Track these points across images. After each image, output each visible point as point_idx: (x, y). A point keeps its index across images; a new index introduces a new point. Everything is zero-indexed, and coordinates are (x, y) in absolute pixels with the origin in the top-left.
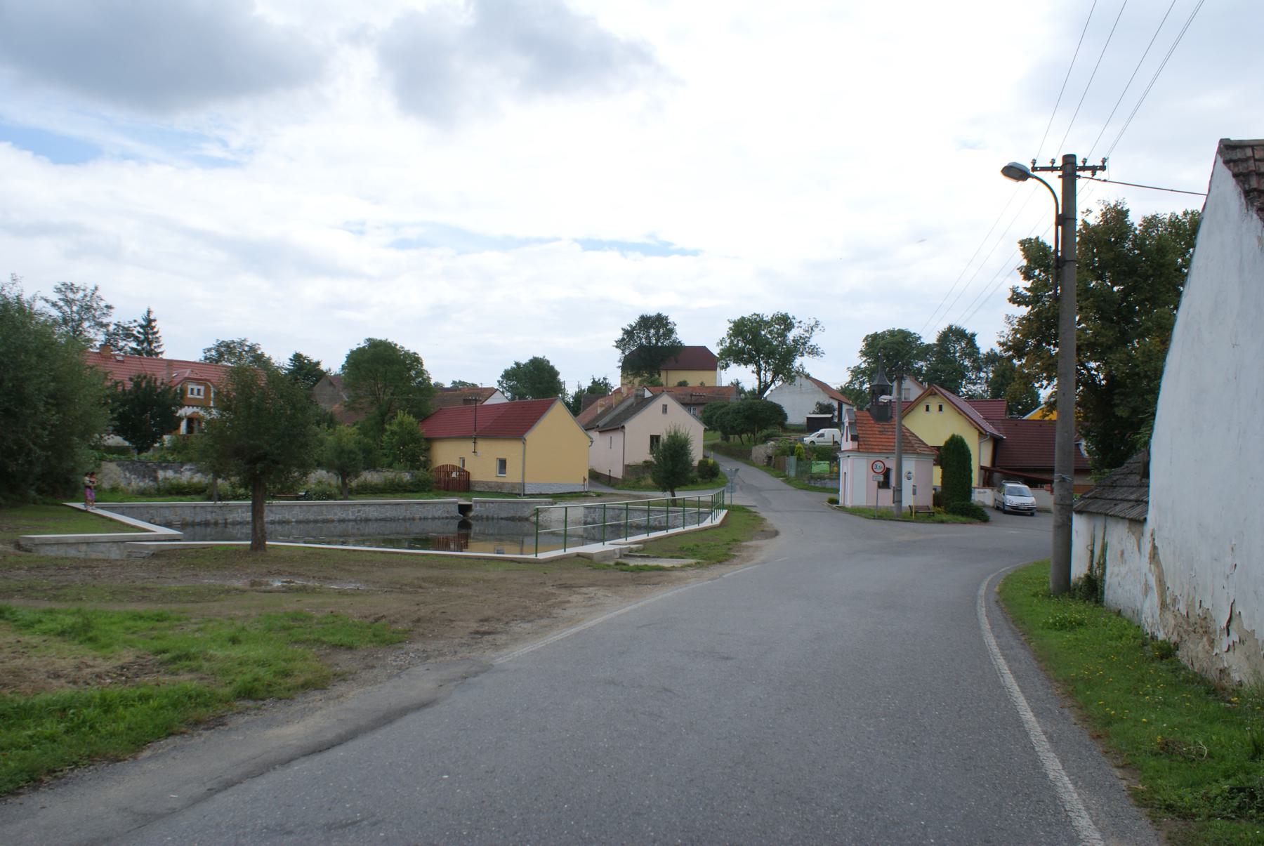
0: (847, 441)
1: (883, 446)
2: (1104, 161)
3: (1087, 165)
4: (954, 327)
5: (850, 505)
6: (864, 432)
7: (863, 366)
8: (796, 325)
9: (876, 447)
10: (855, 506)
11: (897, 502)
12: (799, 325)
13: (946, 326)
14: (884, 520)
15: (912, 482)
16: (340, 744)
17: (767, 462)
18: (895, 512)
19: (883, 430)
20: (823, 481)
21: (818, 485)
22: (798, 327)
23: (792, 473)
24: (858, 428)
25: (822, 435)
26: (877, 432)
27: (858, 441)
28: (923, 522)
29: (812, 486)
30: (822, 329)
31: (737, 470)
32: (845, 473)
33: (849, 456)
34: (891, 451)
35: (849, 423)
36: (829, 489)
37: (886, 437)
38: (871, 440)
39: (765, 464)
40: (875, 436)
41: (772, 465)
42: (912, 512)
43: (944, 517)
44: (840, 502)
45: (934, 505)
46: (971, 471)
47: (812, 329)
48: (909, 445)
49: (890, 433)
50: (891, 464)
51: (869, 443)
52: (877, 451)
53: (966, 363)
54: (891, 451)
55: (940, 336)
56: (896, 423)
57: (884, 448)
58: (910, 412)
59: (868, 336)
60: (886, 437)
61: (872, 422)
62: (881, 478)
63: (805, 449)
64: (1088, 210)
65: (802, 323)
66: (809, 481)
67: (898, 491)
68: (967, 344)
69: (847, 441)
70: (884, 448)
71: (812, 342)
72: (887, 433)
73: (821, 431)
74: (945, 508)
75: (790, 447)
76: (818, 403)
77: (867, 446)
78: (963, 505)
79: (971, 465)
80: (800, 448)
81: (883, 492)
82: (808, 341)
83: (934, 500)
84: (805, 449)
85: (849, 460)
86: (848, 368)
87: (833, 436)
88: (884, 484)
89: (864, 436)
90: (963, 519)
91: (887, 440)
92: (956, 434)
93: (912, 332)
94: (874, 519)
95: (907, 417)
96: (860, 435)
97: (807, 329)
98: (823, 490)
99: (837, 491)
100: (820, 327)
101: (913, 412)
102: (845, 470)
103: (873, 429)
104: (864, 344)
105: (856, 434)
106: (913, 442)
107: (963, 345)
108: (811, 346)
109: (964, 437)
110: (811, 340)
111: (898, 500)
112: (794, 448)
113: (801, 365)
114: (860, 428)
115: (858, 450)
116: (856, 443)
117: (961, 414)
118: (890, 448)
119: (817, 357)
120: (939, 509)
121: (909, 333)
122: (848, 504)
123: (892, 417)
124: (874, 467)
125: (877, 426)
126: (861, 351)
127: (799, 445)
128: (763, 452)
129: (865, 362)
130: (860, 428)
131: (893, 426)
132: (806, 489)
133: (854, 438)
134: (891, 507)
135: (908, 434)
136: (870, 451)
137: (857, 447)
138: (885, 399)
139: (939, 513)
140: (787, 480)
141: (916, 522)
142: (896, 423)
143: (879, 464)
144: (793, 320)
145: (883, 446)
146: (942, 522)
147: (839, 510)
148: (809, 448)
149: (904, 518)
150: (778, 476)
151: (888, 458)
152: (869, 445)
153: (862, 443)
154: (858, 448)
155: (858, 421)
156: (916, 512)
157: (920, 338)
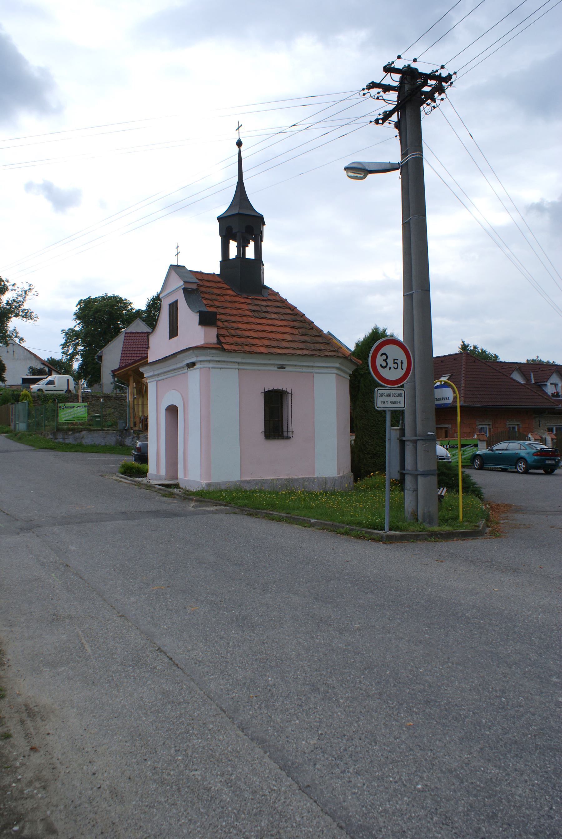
5: (204, 482)
8: (10, 288)
10: (215, 484)
12: (13, 288)
20: (77, 435)
21: (70, 440)
22: (12, 290)
23: (22, 426)
25: (51, 383)
27: (219, 328)
29: (59, 443)
30: (36, 293)
33: (193, 364)
38: (240, 326)
47: (26, 293)
51: (240, 333)
59: (81, 300)
63: (34, 397)
65: (16, 286)
71: (26, 306)
76: (31, 368)
77: (235, 339)
82: (22, 305)
84: (34, 397)
85: (194, 375)
86: (62, 331)
97: (20, 293)
100: (33, 291)
104: (77, 308)
108: (25, 310)
110: (25, 304)
113: (14, 330)
116: (213, 332)
119: (30, 321)
121: (121, 299)
126: (75, 314)
132: (52, 448)
136: (247, 348)
137: (215, 340)
144: (6, 283)
145: (269, 339)
148: (39, 396)
151: (282, 367)
152: (241, 337)
154: (219, 342)
157: (131, 303)
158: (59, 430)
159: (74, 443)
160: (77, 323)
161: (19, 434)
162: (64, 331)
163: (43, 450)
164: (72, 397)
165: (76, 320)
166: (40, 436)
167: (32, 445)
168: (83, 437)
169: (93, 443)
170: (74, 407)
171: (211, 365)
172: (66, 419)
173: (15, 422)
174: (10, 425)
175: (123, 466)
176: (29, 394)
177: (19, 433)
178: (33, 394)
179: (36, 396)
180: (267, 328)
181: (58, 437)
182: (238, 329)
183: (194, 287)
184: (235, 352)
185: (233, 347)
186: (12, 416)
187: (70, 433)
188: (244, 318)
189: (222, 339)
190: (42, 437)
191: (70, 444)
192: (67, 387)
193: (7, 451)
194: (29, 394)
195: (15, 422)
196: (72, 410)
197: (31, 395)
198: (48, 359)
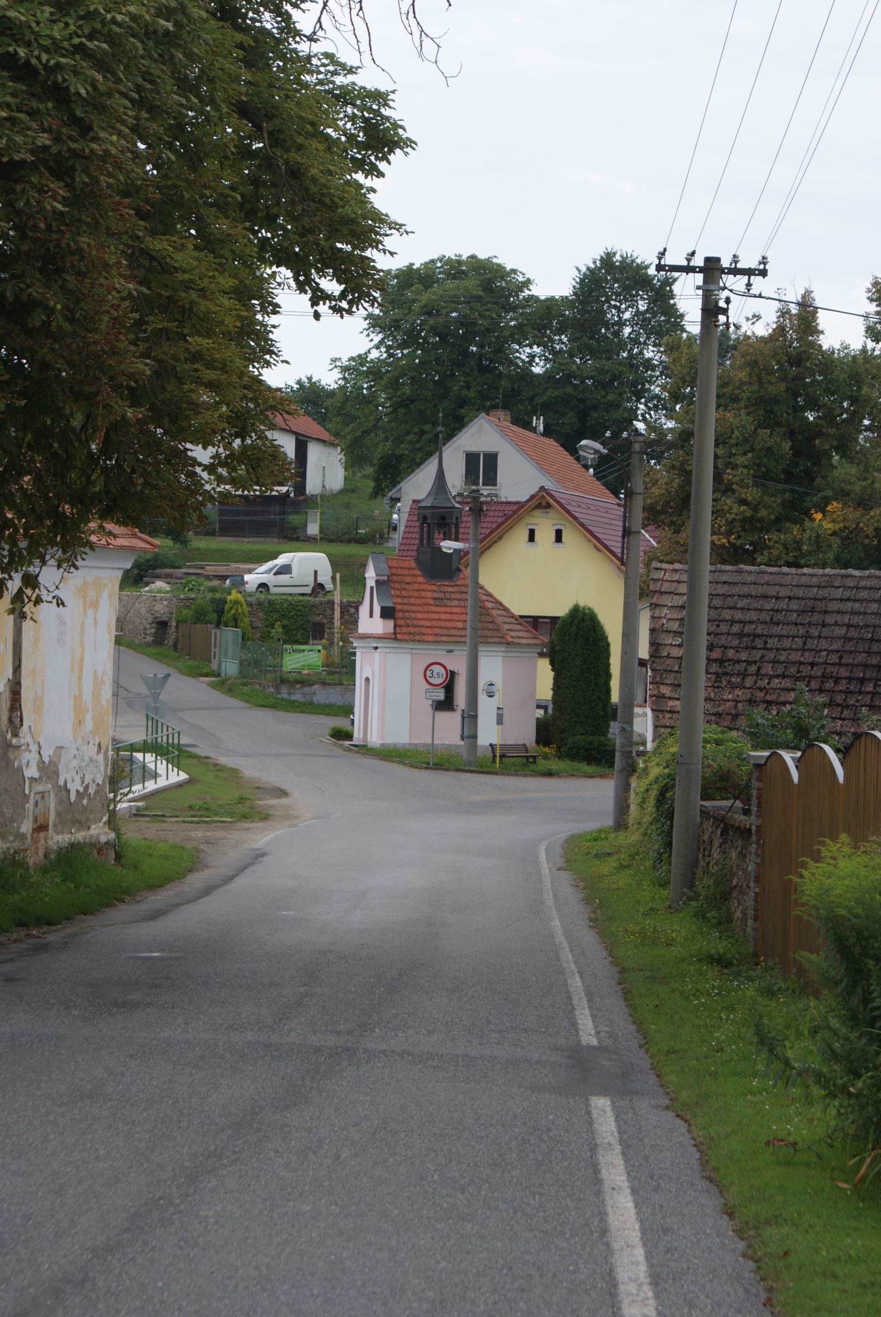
0: (371, 616)
1: (441, 627)
2: (764, 261)
3: (739, 266)
4: (618, 257)
5: (379, 742)
6: (406, 601)
7: (374, 354)
9: (429, 631)
10: (389, 745)
11: (469, 737)
13: (598, 253)
14: (446, 770)
15: (495, 702)
16: (237, 875)
17: (155, 635)
18: (465, 755)
19: (441, 595)
20: (307, 689)
21: (297, 697)
23: (230, 668)
24: (393, 592)
25: (285, 569)
26: (431, 601)
27: (395, 619)
28: (516, 774)
29: (283, 699)
31: (167, 676)
32: (367, 679)
33: (376, 648)
34: (458, 639)
35: (377, 582)
36: (319, 705)
37: (448, 610)
38: (419, 616)
39: (150, 639)
40: (425, 608)
41: (171, 640)
42: (495, 756)
43: (555, 765)
44: (356, 735)
45: (538, 742)
46: (609, 676)
48: (491, 626)
49: (455, 603)
50: (458, 663)
51: (416, 622)
52: (431, 638)
53: (648, 354)
54: (458, 639)
55: (582, 281)
56: (468, 582)
57: (444, 632)
58: (495, 542)
60: (448, 610)
61: (421, 579)
62: (441, 695)
63: (250, 605)
64: (754, 316)
66: (277, 687)
67: (471, 717)
68: (652, 301)
69: (371, 616)
70: (444, 632)
72: (449, 603)
73: (283, 560)
74: (559, 747)
75: (213, 600)
77: (411, 629)
78: (591, 743)
79: (609, 665)
80: (236, 602)
81: (443, 717)
83: (538, 733)
84: (250, 605)
85: (377, 655)
86: (334, 360)
87: (316, 572)
88: (446, 704)
89: (406, 608)
90: (590, 769)
91: (449, 617)
92: (582, 604)
93: (508, 268)
94: (427, 768)
95: (495, 547)
96: (399, 607)
98: (309, 708)
99: (348, 710)
101: (500, 544)
102: (367, 673)
103: (423, 594)
105: (392, 605)
106: (500, 620)
107: (642, 306)
109: (596, 611)
111: (470, 734)
112: (224, 602)
114: (398, 593)
115: (394, 637)
116: (390, 624)
117: (600, 551)
118: (454, 632)
120: (546, 749)
122: (375, 739)
123: (459, 570)
124: (429, 673)
125: (429, 587)
127: (234, 596)
128: (143, 611)
129: (377, 347)
130: (398, 593)
131: (464, 589)
133: (387, 613)
134: (456, 746)
135: (485, 598)
136: (418, 637)
137: (391, 630)
138: (450, 548)
139: (546, 757)
140: (224, 686)
141: (503, 774)
142: (468, 582)
143: (437, 669)
145: (441, 627)
146: (550, 774)
147: (357, 752)
148: (259, 604)
149: (482, 767)
150: (196, 674)
151: (451, 651)
153: (399, 622)
154: (395, 633)
155: (395, 578)
156: (502, 757)
157: (527, 283)
158: (283, 681)
159: (302, 700)
160: (372, 344)
161: (229, 682)
162: (338, 363)
163: (261, 708)
164: (321, 604)
165: (372, 336)
166: (257, 686)
167: (247, 701)
168: (314, 693)
169: (327, 702)
170: (304, 651)
171: (388, 651)
172: (293, 666)
173: (220, 658)
174: (210, 662)
175: (333, 729)
176: (243, 600)
177: (227, 680)
178: (248, 599)
179: (254, 602)
180: (444, 617)
181: (282, 691)
182: (415, 619)
183: (385, 578)
184: (406, 640)
185: (406, 637)
186: (215, 647)
187: (298, 686)
188: (425, 607)
189: (398, 630)
190: (261, 689)
191: (297, 701)
192: (313, 578)
193: (216, 708)
194: (243, 600)
195: (220, 658)
196: (301, 655)
197: (246, 601)
198: (299, 382)
